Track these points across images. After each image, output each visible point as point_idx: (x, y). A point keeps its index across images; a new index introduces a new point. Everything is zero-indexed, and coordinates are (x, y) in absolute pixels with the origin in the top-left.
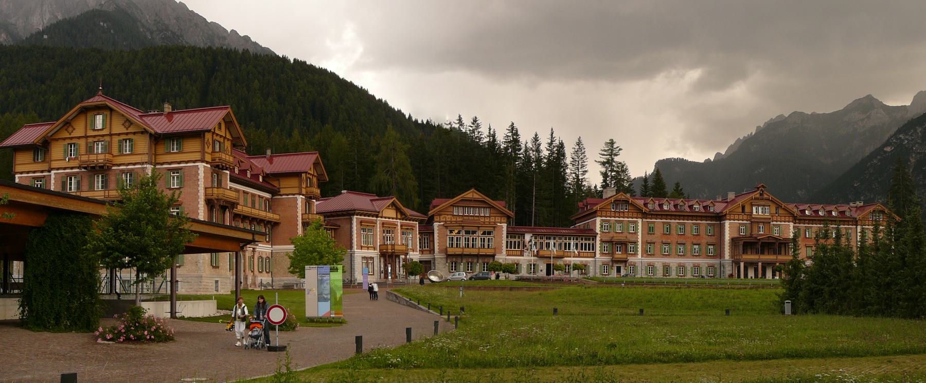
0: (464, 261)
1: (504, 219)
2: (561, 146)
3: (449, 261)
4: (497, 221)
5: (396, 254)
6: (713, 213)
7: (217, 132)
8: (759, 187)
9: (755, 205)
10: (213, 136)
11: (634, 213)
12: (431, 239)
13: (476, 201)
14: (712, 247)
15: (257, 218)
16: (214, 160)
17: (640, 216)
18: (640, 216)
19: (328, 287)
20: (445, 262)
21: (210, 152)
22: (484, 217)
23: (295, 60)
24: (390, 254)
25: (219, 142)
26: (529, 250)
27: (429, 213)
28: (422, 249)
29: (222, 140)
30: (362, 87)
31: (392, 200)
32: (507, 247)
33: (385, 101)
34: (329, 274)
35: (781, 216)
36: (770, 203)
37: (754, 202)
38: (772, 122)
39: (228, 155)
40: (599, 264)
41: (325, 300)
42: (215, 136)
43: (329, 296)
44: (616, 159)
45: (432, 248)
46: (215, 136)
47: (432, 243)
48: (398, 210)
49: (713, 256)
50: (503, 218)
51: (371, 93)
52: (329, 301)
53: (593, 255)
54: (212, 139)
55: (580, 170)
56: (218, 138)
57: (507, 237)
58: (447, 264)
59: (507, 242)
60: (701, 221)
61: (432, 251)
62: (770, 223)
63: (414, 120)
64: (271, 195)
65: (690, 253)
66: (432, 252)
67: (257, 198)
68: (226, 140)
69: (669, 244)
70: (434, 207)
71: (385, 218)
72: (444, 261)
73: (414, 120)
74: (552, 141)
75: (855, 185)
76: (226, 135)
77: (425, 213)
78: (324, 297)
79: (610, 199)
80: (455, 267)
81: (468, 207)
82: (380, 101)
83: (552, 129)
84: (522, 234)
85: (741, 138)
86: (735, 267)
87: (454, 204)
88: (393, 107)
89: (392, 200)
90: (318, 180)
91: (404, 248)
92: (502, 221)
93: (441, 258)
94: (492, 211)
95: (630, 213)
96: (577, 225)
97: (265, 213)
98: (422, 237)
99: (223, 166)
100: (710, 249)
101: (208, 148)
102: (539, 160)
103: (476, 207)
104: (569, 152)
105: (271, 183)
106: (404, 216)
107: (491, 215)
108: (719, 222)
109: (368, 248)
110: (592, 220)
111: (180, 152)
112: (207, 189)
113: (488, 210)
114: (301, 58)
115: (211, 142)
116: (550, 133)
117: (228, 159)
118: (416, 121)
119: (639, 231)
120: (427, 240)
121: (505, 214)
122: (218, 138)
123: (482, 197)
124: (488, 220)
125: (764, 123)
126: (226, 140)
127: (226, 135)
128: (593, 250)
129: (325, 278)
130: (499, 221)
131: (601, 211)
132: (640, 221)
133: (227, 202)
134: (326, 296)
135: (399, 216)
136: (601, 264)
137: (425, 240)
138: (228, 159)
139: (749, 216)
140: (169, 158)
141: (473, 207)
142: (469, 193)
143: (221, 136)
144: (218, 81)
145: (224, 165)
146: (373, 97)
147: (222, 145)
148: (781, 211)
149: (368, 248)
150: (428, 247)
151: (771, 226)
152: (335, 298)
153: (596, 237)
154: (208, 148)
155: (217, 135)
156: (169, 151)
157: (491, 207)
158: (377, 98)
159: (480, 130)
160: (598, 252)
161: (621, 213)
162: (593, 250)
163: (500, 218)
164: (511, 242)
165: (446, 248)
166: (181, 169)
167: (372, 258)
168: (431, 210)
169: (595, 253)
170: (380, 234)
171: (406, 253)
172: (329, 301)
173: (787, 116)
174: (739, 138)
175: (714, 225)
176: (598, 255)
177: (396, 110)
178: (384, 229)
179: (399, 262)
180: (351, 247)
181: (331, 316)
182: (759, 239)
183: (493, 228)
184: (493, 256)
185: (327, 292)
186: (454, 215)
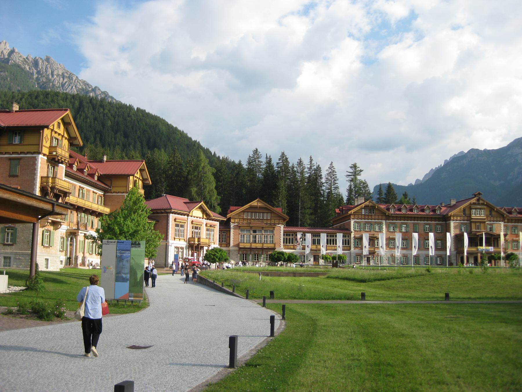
0: (252, 253)
1: (281, 221)
2: (318, 169)
3: (241, 252)
4: (276, 222)
5: (201, 245)
6: (439, 215)
7: (56, 129)
8: (476, 194)
9: (474, 209)
10: (51, 133)
11: (379, 216)
12: (228, 235)
13: (261, 208)
14: (440, 242)
15: (90, 210)
16: (51, 153)
17: (384, 218)
18: (384, 218)
19: (127, 265)
20: (237, 253)
21: (48, 146)
22: (267, 220)
23: (137, 108)
24: (196, 245)
25: (58, 139)
26: (301, 244)
27: (228, 215)
28: (221, 243)
29: (60, 138)
30: (183, 131)
31: (200, 204)
32: (284, 243)
33: (199, 142)
34: (129, 250)
35: (494, 217)
36: (485, 207)
37: (473, 206)
38: (456, 157)
39: (65, 151)
40: (353, 255)
41: (124, 280)
42: (53, 133)
43: (128, 276)
44: (359, 177)
45: (228, 242)
46: (53, 133)
47: (228, 239)
48: (204, 211)
49: (441, 248)
50: (280, 221)
51: (189, 135)
52: (128, 282)
53: (348, 248)
54: (51, 135)
55: (332, 187)
56: (56, 136)
57: (284, 235)
58: (239, 255)
59: (284, 239)
60: (427, 221)
61: (228, 244)
62: (485, 222)
63: (217, 156)
64: (103, 192)
65: (423, 246)
66: (228, 245)
67: (91, 193)
68: (64, 139)
69: (407, 239)
70: (232, 211)
71: (194, 217)
72: (236, 253)
73: (217, 156)
74: (311, 166)
75: (518, 200)
76: (64, 134)
77: (225, 216)
78: (122, 277)
79: (361, 205)
80: (246, 257)
81: (255, 212)
82: (195, 141)
83: (311, 158)
84: (295, 233)
85: (434, 169)
86: (459, 257)
87: (245, 210)
88: (203, 147)
89: (200, 204)
90: (143, 183)
91: (207, 241)
92: (280, 222)
93: (235, 250)
94: (273, 215)
95: (376, 216)
96: (334, 226)
97: (97, 205)
98: (221, 234)
99: (59, 159)
100: (438, 243)
101: (46, 142)
102: (303, 178)
103: (261, 212)
104: (324, 173)
105: (105, 182)
106: (208, 217)
107: (272, 218)
108: (445, 222)
109: (180, 239)
110: (347, 222)
111: (20, 144)
112: (43, 178)
113: (269, 215)
114: (142, 108)
115: (49, 137)
116: (309, 161)
117: (64, 154)
118: (219, 157)
119: (383, 229)
120: (225, 236)
121: (282, 217)
122: (56, 136)
123: (265, 205)
124: (269, 222)
125: (450, 158)
126: (64, 139)
127: (64, 134)
128: (348, 244)
129: (125, 255)
130: (278, 222)
131: (354, 215)
132: (384, 222)
133: (60, 191)
134: (124, 276)
135: (205, 217)
136: (355, 255)
137: (223, 236)
138: (64, 154)
139: (468, 217)
140: (10, 149)
141: (258, 212)
142: (254, 203)
143: (59, 134)
144: (82, 118)
145: (60, 158)
146: (191, 139)
147: (60, 142)
148: (493, 213)
149: (180, 239)
150: (225, 242)
151: (486, 224)
152: (136, 278)
153: (350, 234)
154: (46, 142)
155: (56, 132)
156: (11, 143)
157: (272, 212)
158: (193, 140)
159: (260, 160)
160: (352, 246)
161: (369, 216)
162: (348, 244)
163: (278, 220)
164: (287, 239)
165: (239, 244)
166: (19, 159)
167: (182, 248)
168: (229, 214)
169: (350, 247)
170: (190, 229)
171: (209, 245)
172: (128, 282)
173: (466, 152)
174: (432, 169)
175: (441, 224)
176: (352, 249)
177: (206, 148)
178: (193, 225)
179: (203, 252)
180: (166, 238)
181: (130, 298)
182: (478, 235)
183: (273, 228)
184: (274, 249)
185: (127, 270)
186: (244, 219)
